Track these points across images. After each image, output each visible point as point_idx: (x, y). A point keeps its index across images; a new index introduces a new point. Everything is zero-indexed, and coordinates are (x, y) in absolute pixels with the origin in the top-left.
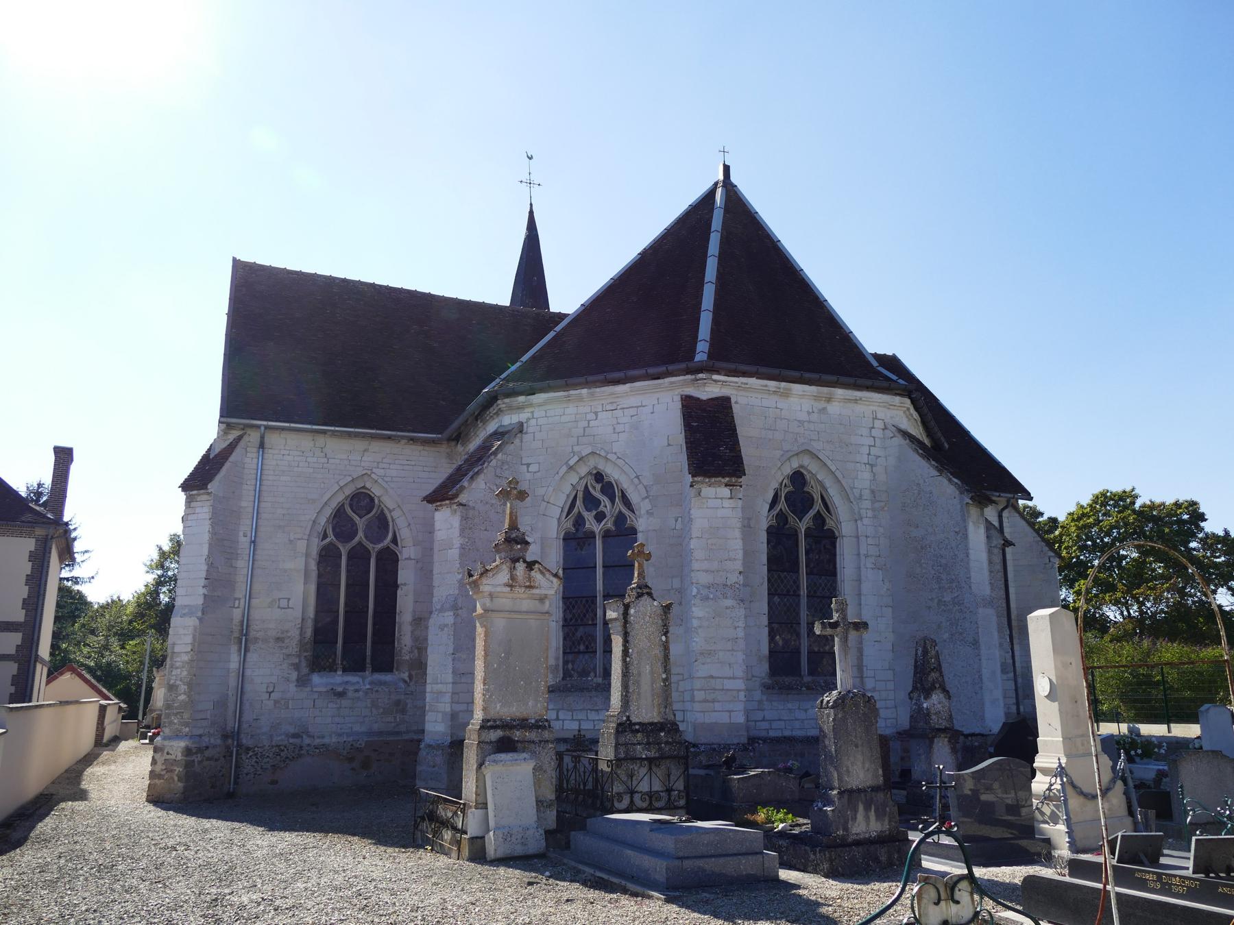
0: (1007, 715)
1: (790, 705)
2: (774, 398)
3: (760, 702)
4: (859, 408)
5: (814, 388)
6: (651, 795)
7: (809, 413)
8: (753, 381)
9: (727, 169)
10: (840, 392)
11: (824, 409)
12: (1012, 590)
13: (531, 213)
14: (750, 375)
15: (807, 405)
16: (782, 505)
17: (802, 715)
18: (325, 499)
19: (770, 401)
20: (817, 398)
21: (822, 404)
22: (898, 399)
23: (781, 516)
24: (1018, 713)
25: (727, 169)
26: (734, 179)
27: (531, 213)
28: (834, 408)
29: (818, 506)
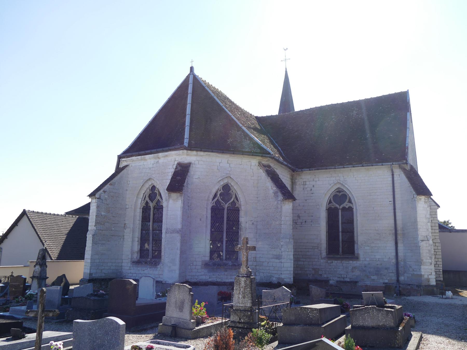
0: (84, 273)
1: (139, 269)
2: (143, 161)
3: (130, 267)
4: (169, 158)
5: (152, 155)
6: (370, 310)
7: (153, 164)
8: (134, 158)
9: (192, 69)
10: (160, 154)
11: (158, 161)
12: (398, 214)
13: (286, 72)
14: (132, 156)
15: (153, 161)
16: (147, 199)
17: (142, 272)
18: (346, 186)
19: (142, 163)
20: (155, 158)
21: (156, 160)
22: (181, 151)
23: (147, 203)
24: (398, 280)
25: (192, 69)
26: (196, 72)
27: (286, 72)
28: (161, 161)
29: (158, 197)
